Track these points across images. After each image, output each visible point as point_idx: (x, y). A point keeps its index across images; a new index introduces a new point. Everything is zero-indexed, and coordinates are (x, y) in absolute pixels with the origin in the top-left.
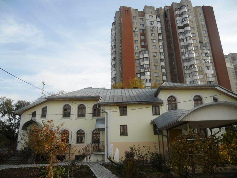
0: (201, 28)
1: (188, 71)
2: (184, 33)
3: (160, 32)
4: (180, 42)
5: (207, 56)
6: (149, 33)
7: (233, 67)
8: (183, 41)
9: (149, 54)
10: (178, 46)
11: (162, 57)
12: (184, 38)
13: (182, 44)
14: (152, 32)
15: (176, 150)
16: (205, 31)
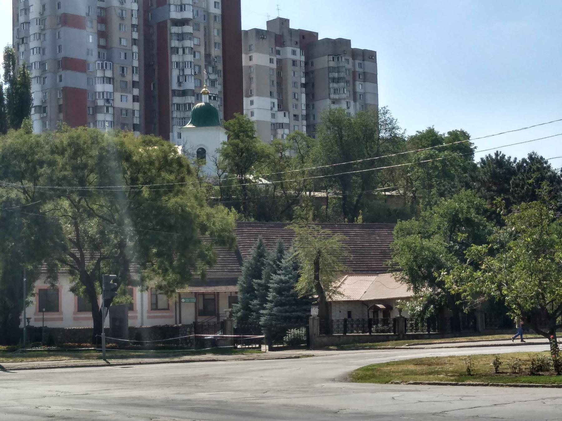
0: (212, 21)
1: (179, 113)
2: (181, 37)
3: (135, 22)
4: (172, 54)
5: (214, 86)
6: (115, 21)
7: (274, 66)
8: (178, 53)
9: (113, 84)
10: (168, 88)
11: (136, 78)
12: (180, 46)
13: (175, 58)
14: (121, 22)
15: (394, 180)
16: (218, 30)
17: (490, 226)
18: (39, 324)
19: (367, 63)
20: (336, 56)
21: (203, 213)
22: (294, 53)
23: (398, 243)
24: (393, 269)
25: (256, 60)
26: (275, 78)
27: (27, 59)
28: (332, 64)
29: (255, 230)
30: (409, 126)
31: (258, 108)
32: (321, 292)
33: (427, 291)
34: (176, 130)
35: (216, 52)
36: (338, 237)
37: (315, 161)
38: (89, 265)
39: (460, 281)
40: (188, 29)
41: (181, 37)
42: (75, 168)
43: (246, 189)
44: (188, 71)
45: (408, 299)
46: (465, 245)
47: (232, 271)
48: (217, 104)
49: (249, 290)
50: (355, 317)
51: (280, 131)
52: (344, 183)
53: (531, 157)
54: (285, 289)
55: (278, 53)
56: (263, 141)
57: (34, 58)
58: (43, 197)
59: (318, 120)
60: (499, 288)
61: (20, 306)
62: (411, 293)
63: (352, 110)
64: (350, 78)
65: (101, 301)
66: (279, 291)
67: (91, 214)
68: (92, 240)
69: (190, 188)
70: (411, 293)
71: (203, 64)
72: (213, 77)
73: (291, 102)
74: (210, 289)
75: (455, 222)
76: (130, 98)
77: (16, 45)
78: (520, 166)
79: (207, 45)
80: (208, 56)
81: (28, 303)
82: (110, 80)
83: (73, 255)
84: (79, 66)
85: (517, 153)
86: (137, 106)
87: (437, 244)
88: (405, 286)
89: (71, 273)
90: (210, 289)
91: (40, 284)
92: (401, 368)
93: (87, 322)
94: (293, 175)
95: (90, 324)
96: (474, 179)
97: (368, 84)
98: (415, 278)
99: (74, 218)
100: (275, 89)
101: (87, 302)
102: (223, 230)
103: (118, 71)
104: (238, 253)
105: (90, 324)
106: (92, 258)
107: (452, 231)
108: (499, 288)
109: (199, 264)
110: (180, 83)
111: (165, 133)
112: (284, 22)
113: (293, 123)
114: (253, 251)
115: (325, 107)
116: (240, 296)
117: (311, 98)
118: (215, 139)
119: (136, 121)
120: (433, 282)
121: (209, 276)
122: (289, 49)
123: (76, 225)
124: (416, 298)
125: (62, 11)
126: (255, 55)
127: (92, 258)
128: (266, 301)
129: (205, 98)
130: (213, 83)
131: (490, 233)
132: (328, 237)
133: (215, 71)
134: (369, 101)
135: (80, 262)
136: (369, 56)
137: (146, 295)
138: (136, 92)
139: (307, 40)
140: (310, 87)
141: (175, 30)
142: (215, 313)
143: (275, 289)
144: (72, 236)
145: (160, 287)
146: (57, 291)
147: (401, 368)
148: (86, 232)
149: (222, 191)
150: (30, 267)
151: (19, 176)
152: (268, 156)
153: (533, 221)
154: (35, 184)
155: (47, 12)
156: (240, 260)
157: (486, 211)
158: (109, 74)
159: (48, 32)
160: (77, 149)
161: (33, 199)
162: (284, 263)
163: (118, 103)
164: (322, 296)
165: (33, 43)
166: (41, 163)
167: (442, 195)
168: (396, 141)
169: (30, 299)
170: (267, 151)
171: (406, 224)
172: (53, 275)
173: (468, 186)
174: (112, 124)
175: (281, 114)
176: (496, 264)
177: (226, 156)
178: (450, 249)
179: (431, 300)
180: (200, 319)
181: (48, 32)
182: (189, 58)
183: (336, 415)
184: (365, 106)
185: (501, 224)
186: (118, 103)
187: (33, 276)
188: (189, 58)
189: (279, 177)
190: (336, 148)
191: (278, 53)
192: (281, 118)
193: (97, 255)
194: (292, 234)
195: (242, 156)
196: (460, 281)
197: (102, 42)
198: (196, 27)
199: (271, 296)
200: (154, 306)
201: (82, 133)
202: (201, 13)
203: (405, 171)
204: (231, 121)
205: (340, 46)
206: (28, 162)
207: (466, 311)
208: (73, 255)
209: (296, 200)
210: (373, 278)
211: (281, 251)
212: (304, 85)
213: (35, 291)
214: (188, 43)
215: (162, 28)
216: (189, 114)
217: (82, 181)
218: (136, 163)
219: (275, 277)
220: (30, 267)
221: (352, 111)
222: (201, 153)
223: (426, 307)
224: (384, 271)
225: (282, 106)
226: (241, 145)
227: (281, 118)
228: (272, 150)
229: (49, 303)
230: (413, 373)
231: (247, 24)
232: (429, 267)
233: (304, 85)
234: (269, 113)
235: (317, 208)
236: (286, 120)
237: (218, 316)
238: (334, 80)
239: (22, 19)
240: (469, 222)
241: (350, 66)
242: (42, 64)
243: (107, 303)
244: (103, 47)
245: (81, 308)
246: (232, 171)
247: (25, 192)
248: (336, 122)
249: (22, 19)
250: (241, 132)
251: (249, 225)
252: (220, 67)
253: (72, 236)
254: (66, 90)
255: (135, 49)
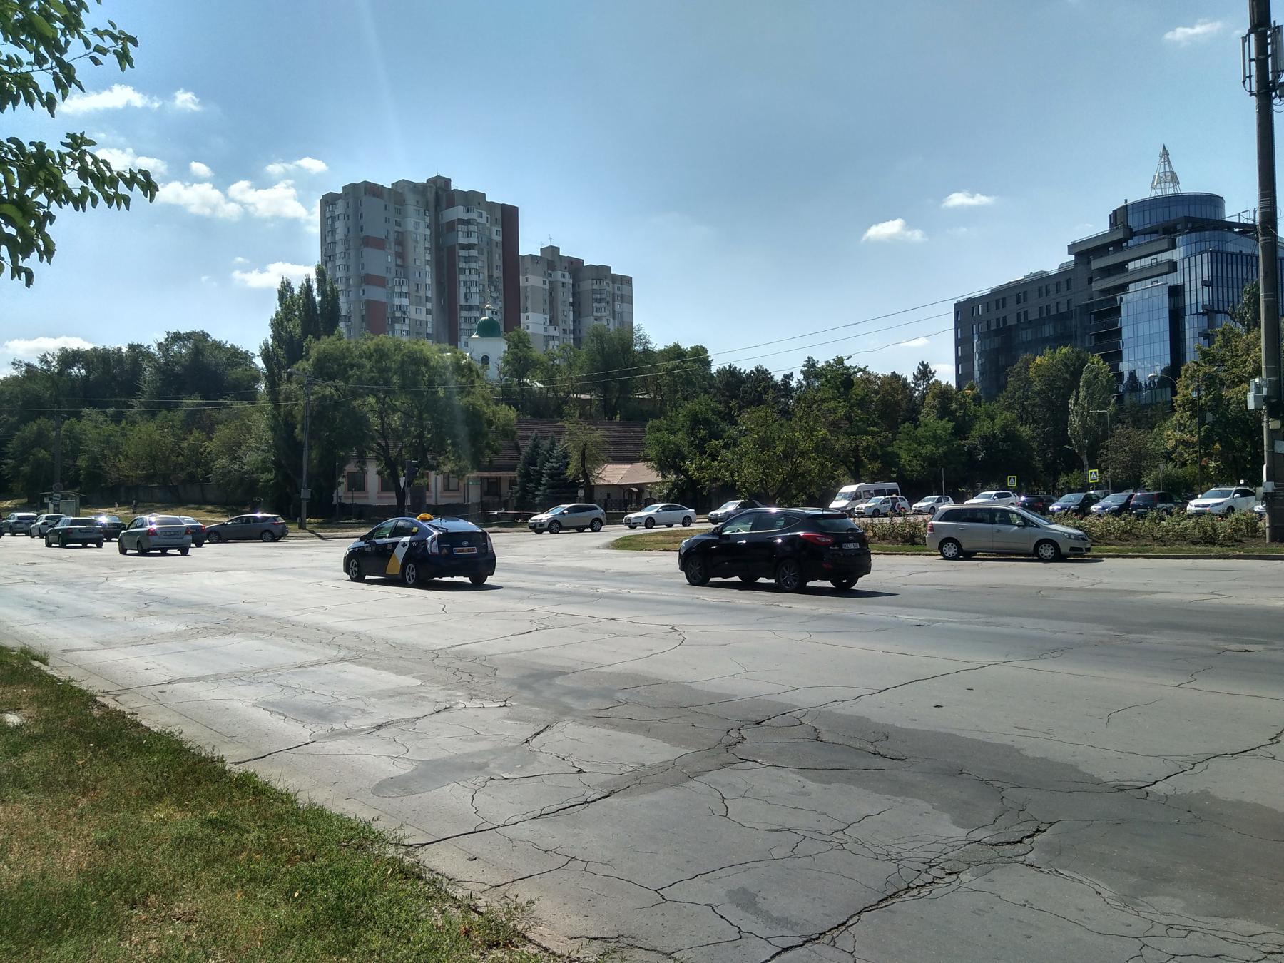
2: (468, 259)
7: (547, 287)
11: (429, 294)
13: (462, 278)
15: (646, 386)
17: (723, 425)
18: (349, 502)
19: (625, 287)
20: (599, 280)
21: (489, 410)
22: (563, 276)
23: (649, 437)
24: (645, 460)
25: (532, 281)
26: (547, 297)
27: (334, 274)
28: (595, 287)
29: (530, 426)
30: (658, 342)
31: (533, 322)
32: (586, 476)
33: (672, 477)
34: (463, 339)
35: (498, 274)
36: (600, 432)
37: (581, 369)
38: (393, 452)
39: (701, 469)
40: (474, 253)
41: (468, 259)
42: (381, 371)
43: (525, 391)
44: (473, 289)
45: (656, 483)
46: (704, 440)
47: (511, 459)
48: (498, 318)
49: (526, 475)
50: (613, 497)
51: (551, 343)
52: (606, 389)
53: (757, 369)
54: (556, 474)
55: (550, 276)
56: (537, 351)
57: (340, 274)
58: (355, 394)
59: (584, 334)
60: (732, 475)
61: (334, 486)
62: (660, 479)
63: (612, 327)
64: (610, 299)
65: (402, 481)
66: (551, 476)
67: (395, 410)
68: (395, 431)
69: (477, 390)
70: (660, 479)
71: (486, 283)
72: (495, 295)
73: (560, 318)
74: (494, 474)
75: (696, 421)
76: (424, 310)
77: (324, 262)
78: (748, 376)
79: (490, 268)
80: (490, 276)
81: (340, 483)
82: (407, 295)
83: (379, 444)
84: (380, 282)
85: (746, 366)
86: (429, 318)
87: (681, 439)
88: (655, 473)
89: (377, 459)
90: (494, 474)
91: (351, 467)
92: (652, 538)
93: (391, 500)
94: (563, 381)
95: (394, 502)
96: (711, 386)
97: (625, 305)
98: (663, 468)
99: (380, 412)
100: (547, 307)
101: (389, 483)
102: (507, 425)
103: (413, 287)
104: (517, 445)
105: (394, 502)
106: (395, 446)
107: (693, 429)
108: (732, 475)
109: (487, 452)
110: (466, 300)
111: (454, 341)
112: (555, 250)
113: (563, 336)
114: (529, 443)
115: (589, 323)
116: (518, 480)
117: (578, 316)
118: (497, 348)
119: (429, 331)
120: (678, 470)
121: (495, 463)
122: (560, 273)
123: (382, 419)
124: (663, 483)
125: (363, 234)
126: (530, 277)
127: (395, 446)
128: (541, 485)
129: (489, 313)
130: (495, 300)
131: (724, 431)
132: (593, 431)
133: (497, 290)
134: (626, 319)
135: (385, 450)
136: (627, 281)
137: (440, 478)
138: (429, 306)
139: (574, 266)
140: (576, 305)
141: (462, 253)
142: (498, 494)
143: (548, 475)
144: (378, 428)
145: (453, 472)
146: (364, 473)
147: (652, 538)
148: (390, 424)
149: (503, 392)
150: (342, 454)
151: (332, 377)
152: (542, 364)
153: (760, 421)
154: (346, 383)
155: (351, 235)
156: (518, 450)
157: (720, 412)
158: (405, 289)
159: (352, 252)
160: (380, 354)
161: (345, 396)
162: (555, 453)
163: (413, 315)
164: (587, 481)
165: (339, 261)
166: (352, 366)
167: (685, 399)
168: (647, 352)
169: (341, 480)
170: (542, 359)
171: (657, 422)
172: (362, 460)
173: (706, 392)
174: (408, 333)
175: (552, 328)
176: (729, 455)
177: (507, 363)
178: (691, 443)
179: (675, 485)
180: (485, 499)
181: (352, 252)
182: (474, 278)
183: (453, 714)
184: (622, 323)
185: (734, 423)
186: (413, 315)
187: (345, 461)
188: (474, 278)
189: (551, 382)
190: (598, 357)
191: (550, 276)
192: (552, 331)
193: (400, 445)
194: (562, 429)
195: (520, 363)
196: (701, 469)
197: (399, 262)
198: (481, 252)
199: (544, 481)
200: (446, 488)
201: (385, 340)
202: (485, 240)
203: (655, 378)
204: (512, 333)
205: (602, 272)
206: (339, 365)
207: (705, 493)
208: (379, 444)
209: (565, 401)
210: (629, 466)
211: (553, 443)
212: (572, 304)
213: (346, 473)
214: (473, 265)
215: (451, 251)
216: (475, 326)
217: (387, 382)
218: (434, 368)
219: (548, 465)
220: (342, 454)
221: (612, 328)
222: (486, 360)
223: (671, 491)
224: (637, 461)
225: (553, 321)
226: (520, 354)
227: (552, 331)
228: (545, 359)
229: (358, 484)
230: (662, 542)
231: (523, 251)
232: (675, 457)
233: (572, 304)
234: (542, 327)
235: (583, 408)
236: (556, 334)
237: (500, 496)
238: (597, 301)
239: (329, 240)
240: (707, 422)
241: (610, 289)
242: (347, 279)
243: (409, 483)
244: (401, 266)
245: (384, 487)
246: (511, 376)
247: (337, 390)
248: (599, 336)
249: (329, 240)
250: (520, 343)
251: (527, 421)
252: (501, 287)
253: (378, 428)
254: (369, 303)
255: (428, 268)
